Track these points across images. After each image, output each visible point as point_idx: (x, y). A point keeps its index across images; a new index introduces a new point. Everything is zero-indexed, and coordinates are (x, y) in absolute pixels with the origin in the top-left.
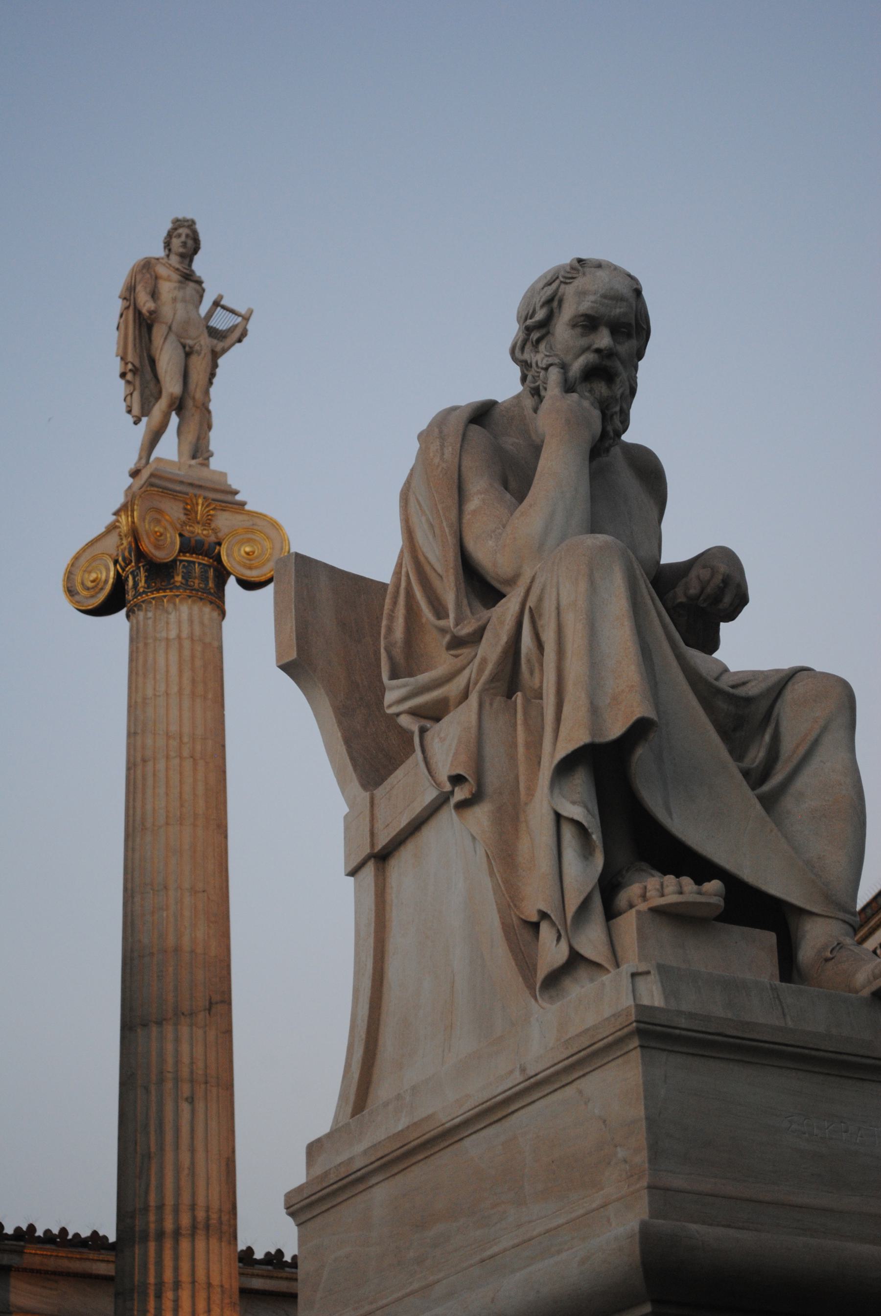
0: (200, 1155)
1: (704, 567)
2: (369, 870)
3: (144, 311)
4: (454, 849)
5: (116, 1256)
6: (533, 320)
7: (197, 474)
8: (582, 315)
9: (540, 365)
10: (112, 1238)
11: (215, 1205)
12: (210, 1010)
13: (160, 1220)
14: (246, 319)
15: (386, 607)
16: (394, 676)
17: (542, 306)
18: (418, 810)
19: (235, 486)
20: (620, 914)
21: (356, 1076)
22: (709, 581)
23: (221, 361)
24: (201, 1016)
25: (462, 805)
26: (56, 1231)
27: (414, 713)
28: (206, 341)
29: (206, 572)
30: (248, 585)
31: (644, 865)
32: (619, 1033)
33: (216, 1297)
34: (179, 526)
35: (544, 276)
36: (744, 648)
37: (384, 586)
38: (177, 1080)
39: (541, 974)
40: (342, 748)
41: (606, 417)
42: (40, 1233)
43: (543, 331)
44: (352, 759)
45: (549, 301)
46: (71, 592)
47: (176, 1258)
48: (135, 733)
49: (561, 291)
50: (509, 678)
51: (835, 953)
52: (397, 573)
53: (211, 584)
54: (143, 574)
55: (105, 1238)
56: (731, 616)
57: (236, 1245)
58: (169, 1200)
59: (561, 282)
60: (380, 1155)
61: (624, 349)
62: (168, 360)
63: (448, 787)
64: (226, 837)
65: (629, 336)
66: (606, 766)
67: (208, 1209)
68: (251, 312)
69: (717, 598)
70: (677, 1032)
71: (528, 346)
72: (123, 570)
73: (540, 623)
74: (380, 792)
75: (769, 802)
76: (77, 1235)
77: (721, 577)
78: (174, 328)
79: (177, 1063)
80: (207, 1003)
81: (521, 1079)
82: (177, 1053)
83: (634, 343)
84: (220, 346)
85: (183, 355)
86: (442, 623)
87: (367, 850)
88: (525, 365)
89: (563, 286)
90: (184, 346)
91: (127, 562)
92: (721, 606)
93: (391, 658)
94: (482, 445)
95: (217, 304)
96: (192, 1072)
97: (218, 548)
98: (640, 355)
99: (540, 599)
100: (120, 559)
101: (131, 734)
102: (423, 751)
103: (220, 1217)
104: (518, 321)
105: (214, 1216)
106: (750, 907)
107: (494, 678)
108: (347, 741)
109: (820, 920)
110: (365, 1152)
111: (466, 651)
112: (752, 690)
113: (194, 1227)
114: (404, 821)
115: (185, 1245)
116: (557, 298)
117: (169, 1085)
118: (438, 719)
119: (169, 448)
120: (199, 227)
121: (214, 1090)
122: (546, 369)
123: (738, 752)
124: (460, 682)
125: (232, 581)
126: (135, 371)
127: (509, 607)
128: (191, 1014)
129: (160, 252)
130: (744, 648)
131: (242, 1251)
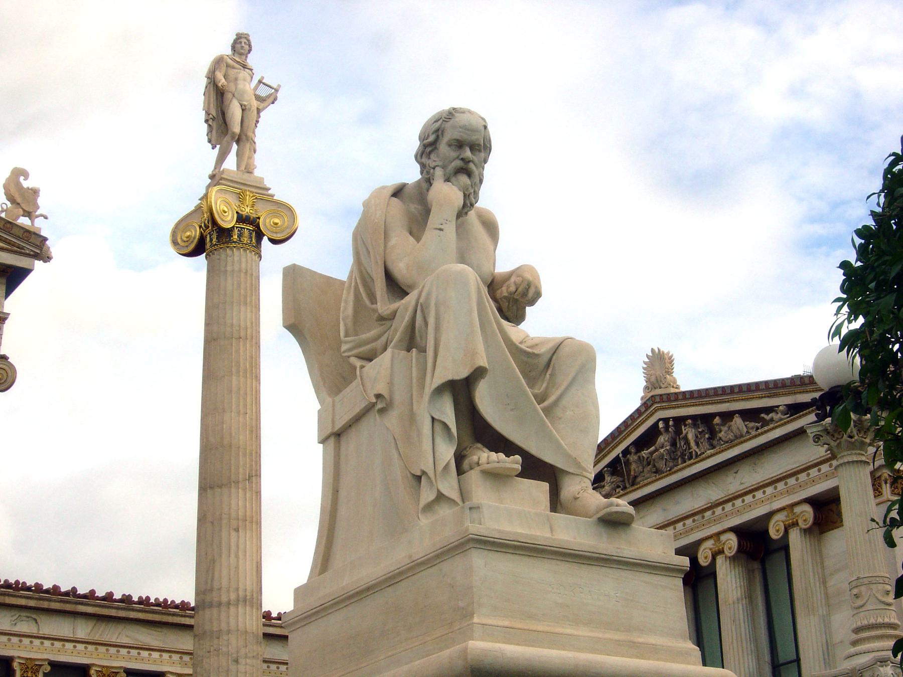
2: (332, 441)
3: (220, 85)
7: (245, 178)
14: (277, 91)
19: (268, 186)
20: (464, 472)
23: (262, 114)
26: (161, 600)
28: (255, 103)
29: (251, 234)
30: (274, 242)
31: (479, 445)
35: (434, 116)
36: (538, 325)
37: (342, 283)
42: (152, 600)
45: (437, 130)
46: (175, 243)
50: (412, 340)
52: (350, 277)
53: (254, 240)
54: (215, 236)
55: (188, 603)
62: (235, 112)
63: (374, 400)
66: (461, 391)
68: (279, 86)
74: (337, 399)
76: (173, 602)
84: (262, 106)
86: (374, 306)
88: (423, 166)
91: (207, 227)
93: (345, 325)
95: (260, 82)
98: (485, 161)
101: (207, 324)
102: (361, 379)
104: (420, 139)
107: (400, 341)
111: (388, 323)
117: (224, 522)
118: (370, 360)
119: (231, 163)
120: (251, 38)
122: (434, 168)
124: (383, 339)
125: (265, 238)
126: (213, 119)
129: (229, 52)
130: (538, 325)
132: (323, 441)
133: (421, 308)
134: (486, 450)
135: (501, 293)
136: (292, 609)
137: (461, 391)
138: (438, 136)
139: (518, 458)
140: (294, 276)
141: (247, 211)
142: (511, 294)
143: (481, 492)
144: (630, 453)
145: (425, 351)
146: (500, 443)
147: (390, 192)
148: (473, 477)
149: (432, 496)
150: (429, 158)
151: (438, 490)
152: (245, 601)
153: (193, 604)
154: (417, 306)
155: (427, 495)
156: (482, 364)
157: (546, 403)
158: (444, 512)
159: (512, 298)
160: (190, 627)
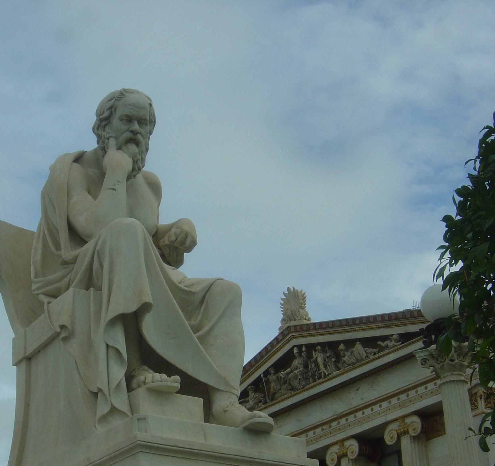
2: (24, 364)
6: (103, 116)
8: (125, 115)
9: (106, 137)
15: (34, 244)
17: (107, 110)
20: (133, 390)
22: (179, 235)
31: (146, 367)
35: (108, 96)
36: (194, 268)
41: (135, 162)
43: (108, 121)
45: (111, 108)
49: (115, 104)
50: (90, 281)
59: (116, 100)
63: (59, 330)
66: (131, 323)
69: (183, 243)
86: (59, 252)
87: (21, 356)
88: (99, 137)
93: (35, 268)
98: (151, 133)
102: (48, 312)
112: (197, 289)
118: (56, 297)
122: (108, 139)
124: (66, 280)
127: (89, 247)
130: (194, 268)
133: (97, 254)
134: (151, 371)
137: (131, 323)
138: (111, 113)
139: (177, 377)
143: (147, 406)
144: (270, 374)
145: (101, 290)
147: (72, 158)
148: (141, 393)
149: (107, 409)
150: (104, 131)
151: (112, 405)
154: (94, 252)
155: (103, 409)
156: (148, 301)
157: (201, 333)
158: (117, 422)
159: (173, 245)
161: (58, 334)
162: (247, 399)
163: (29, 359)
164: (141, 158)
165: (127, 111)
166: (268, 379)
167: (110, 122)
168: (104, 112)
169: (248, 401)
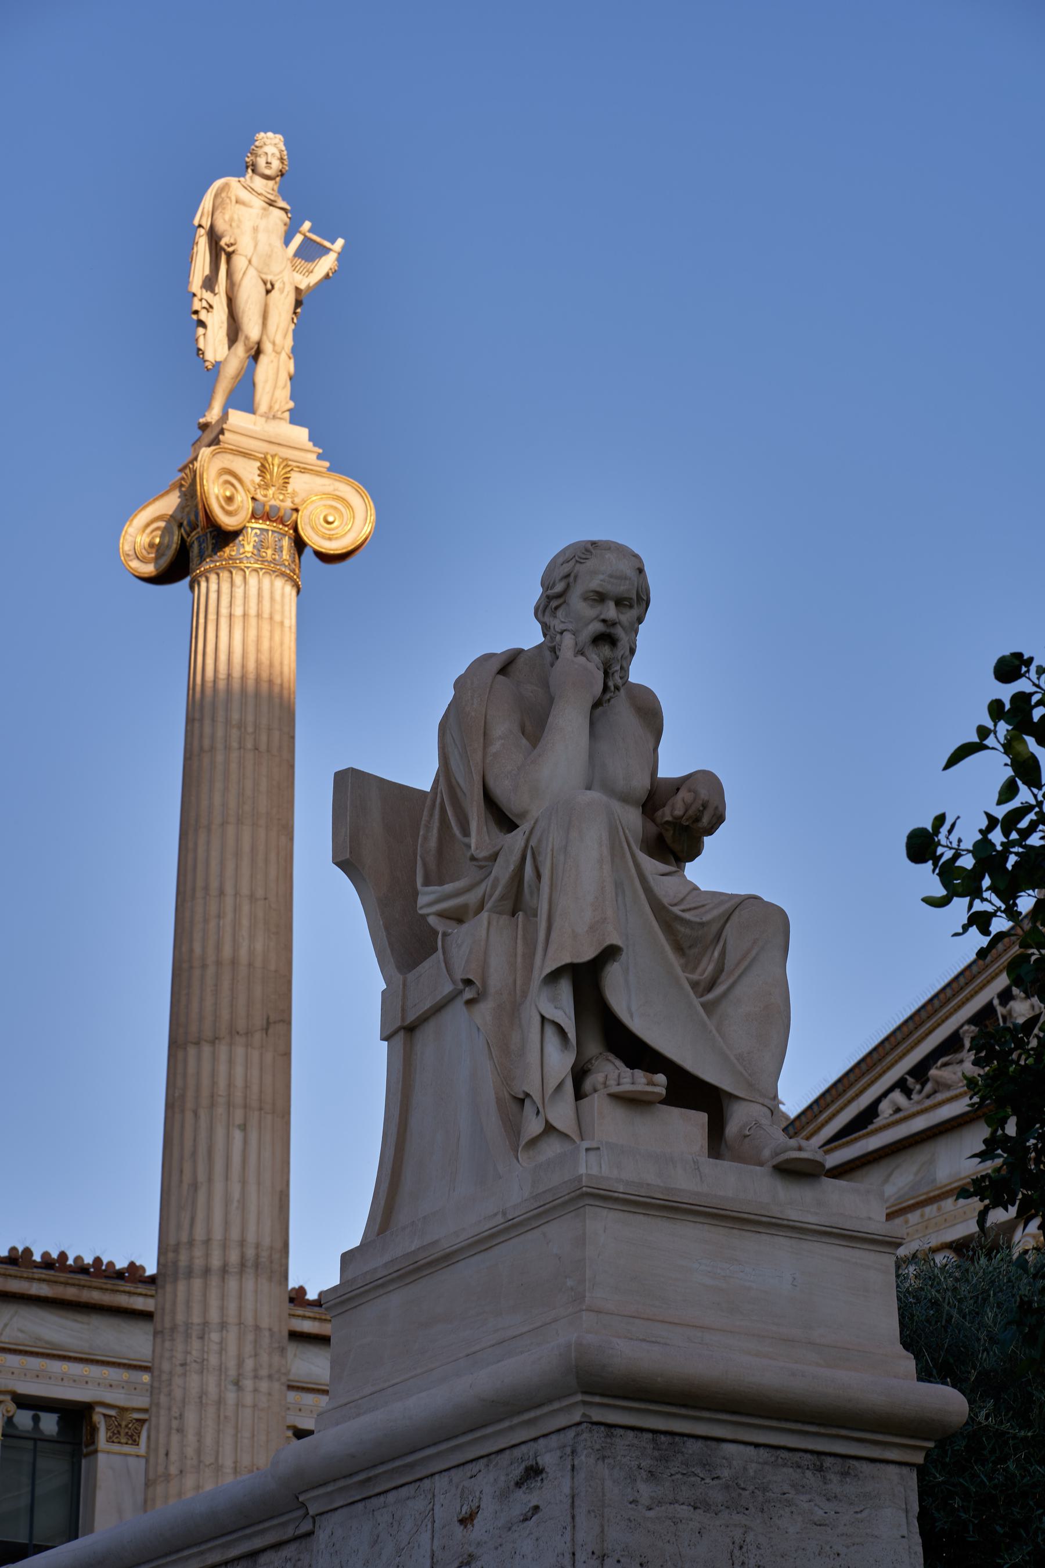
0: (252, 1188)
1: (690, 791)
2: (400, 1037)
4: (462, 1034)
5: (156, 1291)
10: (151, 1269)
11: (266, 1242)
12: (267, 1030)
13: (207, 1256)
16: (427, 883)
18: (439, 998)
20: (586, 1096)
21: (383, 1203)
24: (257, 1037)
25: (470, 1002)
26: (55, 1255)
27: (441, 915)
32: (573, 1194)
33: (266, 1340)
34: (252, 489)
38: (229, 1105)
39: (523, 1142)
40: (383, 934)
44: (391, 944)
47: (223, 1297)
48: (193, 720)
49: (576, 569)
50: (516, 901)
51: (752, 1131)
56: (710, 831)
57: (287, 1285)
58: (217, 1234)
60: (396, 1268)
61: (627, 617)
63: (461, 986)
64: (292, 839)
65: (631, 607)
66: (586, 979)
67: (258, 1246)
69: (697, 819)
70: (616, 1195)
71: (547, 613)
72: (189, 535)
73: (540, 859)
74: (411, 976)
75: (709, 1008)
77: (701, 802)
78: (254, 261)
79: (230, 1085)
80: (265, 1022)
81: (502, 1221)
82: (230, 1076)
83: (634, 613)
85: (264, 292)
86: (466, 840)
87: (398, 1024)
88: (546, 629)
89: (578, 565)
90: (265, 283)
91: (193, 527)
92: (700, 825)
94: (505, 695)
96: (245, 1098)
97: (295, 515)
98: (640, 620)
99: (540, 841)
100: (185, 523)
102: (444, 953)
103: (271, 1256)
105: (265, 1254)
106: (688, 1091)
107: (502, 898)
108: (387, 928)
109: (745, 1104)
110: (385, 1265)
113: (243, 1265)
114: (427, 1005)
115: (232, 1284)
116: (572, 575)
117: (220, 1110)
118: (460, 921)
121: (269, 1117)
123: (690, 965)
124: (479, 892)
128: (247, 1034)
131: (293, 1289)
132: (386, 1038)
133: (530, 852)
134: (619, 1063)
135: (663, 815)
136: (338, 1283)
137: (586, 979)
138: (568, 586)
139: (661, 1078)
140: (353, 788)
141: (272, 498)
142: (675, 818)
143: (610, 1123)
144: (1012, 998)
145: (536, 915)
146: (637, 1053)
147: (496, 665)
148: (597, 1103)
150: (555, 617)
151: (547, 1122)
152: (257, 1265)
153: (151, 1269)
154: (526, 847)
155: (534, 1127)
156: (615, 942)
157: (710, 996)
158: (552, 1148)
159: (679, 820)
160: (146, 1316)
161: (461, 992)
162: (959, 1056)
163: (410, 1029)
164: (622, 668)
165: (595, 584)
166: (1010, 1013)
167: (565, 602)
168: (554, 585)
169: (961, 1061)
